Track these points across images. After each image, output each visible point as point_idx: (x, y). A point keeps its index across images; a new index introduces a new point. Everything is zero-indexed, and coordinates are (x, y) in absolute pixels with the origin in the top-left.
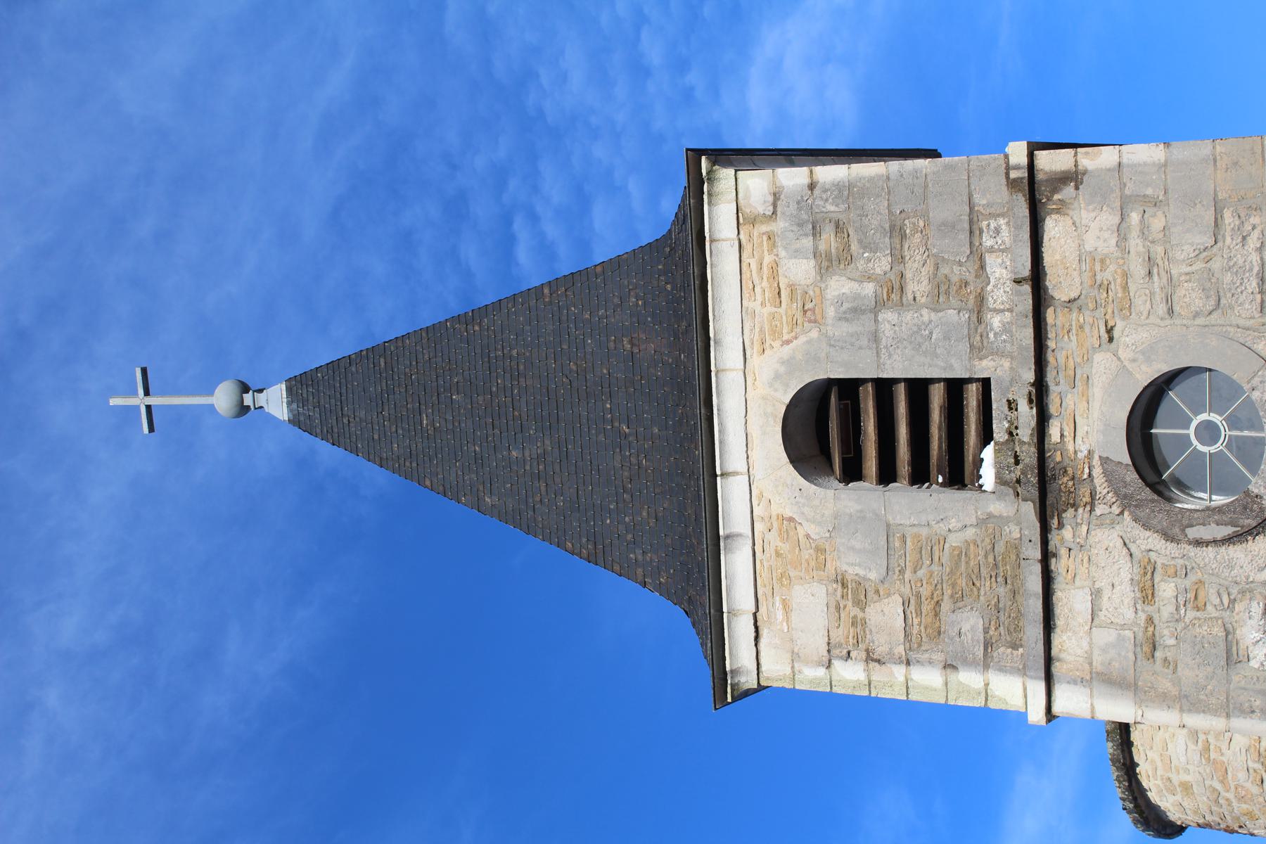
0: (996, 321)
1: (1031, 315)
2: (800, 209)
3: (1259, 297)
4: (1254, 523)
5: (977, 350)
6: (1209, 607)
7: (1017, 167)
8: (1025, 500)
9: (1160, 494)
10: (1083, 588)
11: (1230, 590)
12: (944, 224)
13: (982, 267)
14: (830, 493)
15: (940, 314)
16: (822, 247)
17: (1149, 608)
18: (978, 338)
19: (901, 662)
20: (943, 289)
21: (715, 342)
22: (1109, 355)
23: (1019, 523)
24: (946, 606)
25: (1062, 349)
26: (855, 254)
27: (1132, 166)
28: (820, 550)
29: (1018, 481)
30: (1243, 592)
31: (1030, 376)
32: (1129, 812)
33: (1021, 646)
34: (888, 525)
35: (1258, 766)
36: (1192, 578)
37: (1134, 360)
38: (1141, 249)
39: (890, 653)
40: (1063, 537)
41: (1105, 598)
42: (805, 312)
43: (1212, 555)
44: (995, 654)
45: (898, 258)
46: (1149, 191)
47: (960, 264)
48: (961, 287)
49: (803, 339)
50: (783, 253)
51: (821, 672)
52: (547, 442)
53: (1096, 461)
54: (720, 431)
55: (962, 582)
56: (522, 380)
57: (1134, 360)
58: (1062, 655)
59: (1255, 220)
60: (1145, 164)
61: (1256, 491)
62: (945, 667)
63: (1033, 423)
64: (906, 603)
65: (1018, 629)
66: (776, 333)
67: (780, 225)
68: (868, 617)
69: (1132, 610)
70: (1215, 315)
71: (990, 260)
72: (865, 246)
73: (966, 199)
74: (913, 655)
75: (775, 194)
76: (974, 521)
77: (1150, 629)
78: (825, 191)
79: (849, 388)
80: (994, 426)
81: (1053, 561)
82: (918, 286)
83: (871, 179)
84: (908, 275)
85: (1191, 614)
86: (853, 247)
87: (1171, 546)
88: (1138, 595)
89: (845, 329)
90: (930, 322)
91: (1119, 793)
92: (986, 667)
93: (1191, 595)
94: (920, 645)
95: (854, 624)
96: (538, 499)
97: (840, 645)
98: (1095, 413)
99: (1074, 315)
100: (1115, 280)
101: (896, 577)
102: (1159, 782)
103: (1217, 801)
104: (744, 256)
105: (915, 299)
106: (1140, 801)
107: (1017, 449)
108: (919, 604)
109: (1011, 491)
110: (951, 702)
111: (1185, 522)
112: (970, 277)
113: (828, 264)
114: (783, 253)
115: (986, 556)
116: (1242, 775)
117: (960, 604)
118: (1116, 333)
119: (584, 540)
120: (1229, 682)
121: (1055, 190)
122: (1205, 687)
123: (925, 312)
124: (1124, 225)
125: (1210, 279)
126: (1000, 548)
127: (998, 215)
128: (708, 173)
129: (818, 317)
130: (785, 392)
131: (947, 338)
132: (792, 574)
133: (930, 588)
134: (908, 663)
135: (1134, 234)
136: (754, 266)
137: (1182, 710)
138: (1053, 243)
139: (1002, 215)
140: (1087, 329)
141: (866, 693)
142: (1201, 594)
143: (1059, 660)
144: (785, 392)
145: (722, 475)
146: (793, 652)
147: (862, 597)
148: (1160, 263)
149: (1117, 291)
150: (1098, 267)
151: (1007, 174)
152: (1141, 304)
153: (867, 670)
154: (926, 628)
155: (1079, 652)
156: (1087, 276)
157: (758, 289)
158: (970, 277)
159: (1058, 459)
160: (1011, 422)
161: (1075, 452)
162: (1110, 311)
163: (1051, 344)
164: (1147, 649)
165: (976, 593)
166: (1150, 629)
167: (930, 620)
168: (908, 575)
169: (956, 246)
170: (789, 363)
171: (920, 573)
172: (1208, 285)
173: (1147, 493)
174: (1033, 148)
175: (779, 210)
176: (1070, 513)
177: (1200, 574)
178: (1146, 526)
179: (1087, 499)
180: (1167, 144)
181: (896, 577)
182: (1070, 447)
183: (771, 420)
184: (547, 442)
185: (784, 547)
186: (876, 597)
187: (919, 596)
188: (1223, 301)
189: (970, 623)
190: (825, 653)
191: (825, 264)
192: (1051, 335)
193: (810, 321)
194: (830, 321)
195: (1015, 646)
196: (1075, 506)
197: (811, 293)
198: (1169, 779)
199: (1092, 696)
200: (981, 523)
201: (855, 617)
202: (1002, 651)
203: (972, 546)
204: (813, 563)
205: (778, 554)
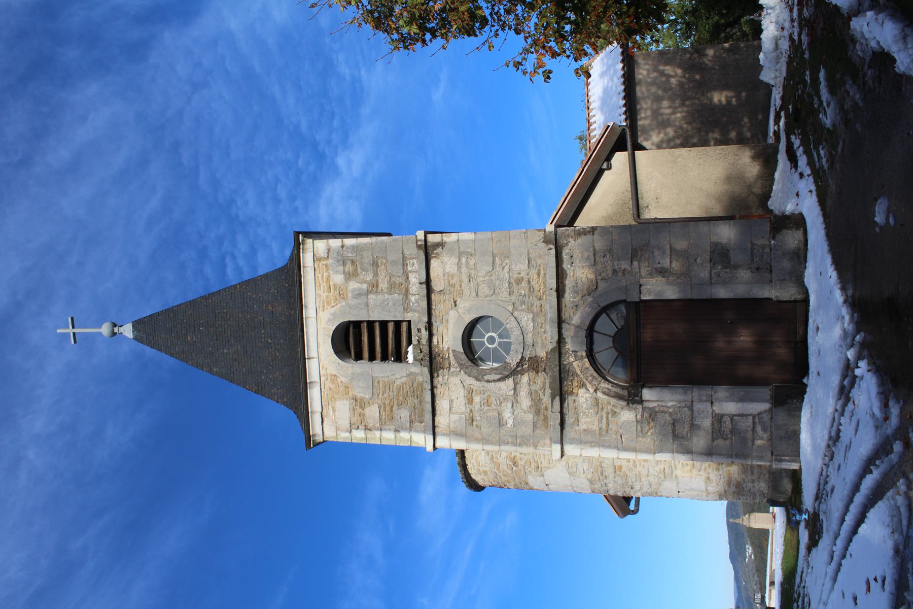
0: (413, 299)
1: (426, 296)
2: (338, 255)
3: (509, 290)
4: (508, 373)
5: (406, 309)
6: (493, 405)
7: (420, 240)
8: (424, 366)
9: (474, 363)
10: (446, 399)
11: (500, 398)
12: (393, 261)
13: (408, 278)
14: (350, 365)
15: (392, 296)
16: (347, 270)
17: (471, 406)
18: (406, 305)
19: (378, 430)
20: (393, 286)
21: (305, 307)
22: (455, 311)
23: (422, 375)
24: (395, 408)
25: (437, 309)
26: (359, 272)
27: (463, 241)
28: (347, 387)
29: (422, 359)
30: (504, 399)
31: (426, 319)
32: (465, 483)
33: (424, 422)
34: (373, 377)
35: (511, 463)
36: (486, 394)
37: (464, 313)
38: (466, 271)
39: (374, 426)
40: (439, 380)
41: (455, 403)
42: (340, 295)
43: (493, 386)
44: (414, 425)
45: (376, 274)
46: (469, 250)
47: (399, 277)
48: (399, 285)
49: (339, 305)
50: (331, 272)
51: (348, 434)
52: (239, 346)
53: (451, 351)
54: (307, 342)
55: (401, 398)
56: (228, 322)
57: (464, 313)
58: (439, 425)
59: (507, 261)
60: (467, 240)
61: (509, 361)
62: (395, 431)
63: (427, 337)
64: (380, 407)
65: (422, 416)
66: (328, 303)
67: (330, 261)
68: (365, 413)
69: (465, 407)
70: (493, 296)
71: (410, 275)
72: (363, 270)
73: (401, 252)
74: (382, 427)
75: (328, 249)
76: (405, 375)
77: (471, 414)
78: (348, 248)
79: (357, 324)
80: (413, 339)
81: (435, 389)
82: (383, 285)
83: (365, 244)
84: (380, 281)
85: (486, 408)
86: (358, 270)
87: (478, 383)
88: (467, 401)
89: (356, 301)
90: (388, 299)
91: (461, 476)
92: (411, 430)
93: (486, 401)
94: (385, 423)
95: (360, 415)
96: (235, 368)
97: (355, 424)
98: (450, 334)
99: (442, 296)
100: (457, 283)
101: (376, 397)
102: (475, 471)
103: (496, 477)
104: (317, 272)
105: (382, 290)
106: (468, 478)
107: (421, 347)
108: (385, 407)
109: (419, 363)
110: (398, 444)
111: (483, 373)
112: (403, 282)
113: (349, 276)
114: (331, 272)
115: (410, 388)
116: (505, 467)
117: (401, 407)
118: (457, 303)
119: (254, 385)
120: (500, 432)
121: (435, 249)
122: (491, 435)
123: (386, 295)
124: (460, 263)
125: (491, 283)
126: (415, 385)
127: (413, 258)
128: (302, 241)
129: (345, 297)
130: (333, 326)
131: (394, 305)
132: (336, 396)
133: (389, 401)
134: (381, 430)
135: (464, 266)
136: (320, 277)
137: (483, 444)
138: (434, 269)
139: (415, 258)
140: (447, 301)
141: (365, 442)
142: (489, 400)
143: (438, 427)
144: (333, 326)
145: (308, 358)
146: (336, 427)
147: (363, 405)
148: (473, 277)
149: (457, 286)
150: (450, 278)
151: (417, 243)
152: (466, 292)
153: (365, 433)
154: (387, 416)
155: (445, 423)
156: (446, 281)
157: (322, 286)
158: (403, 282)
159: (437, 351)
160: (419, 337)
161: (443, 348)
162: (455, 295)
163: (434, 307)
164: (470, 421)
165: (406, 402)
166: (471, 414)
167: (389, 413)
168: (381, 396)
169: (398, 270)
170: (334, 315)
171: (385, 395)
172: (490, 285)
173: (469, 363)
174: (426, 233)
175: (330, 255)
176: (441, 371)
177: (489, 393)
178: (469, 376)
179: (447, 366)
180: (475, 233)
181: (376, 397)
182: (441, 346)
183: (327, 337)
184: (239, 346)
185: (333, 386)
186: (368, 405)
187: (384, 404)
188: (496, 291)
189: (404, 414)
190: (349, 427)
191: (348, 276)
192: (433, 304)
193: (342, 299)
194: (349, 298)
195: (421, 422)
196: (443, 368)
197: (342, 287)
198: (479, 470)
199: (450, 440)
200: (408, 375)
201: (360, 413)
202: (416, 424)
203: (405, 385)
204: (344, 392)
205: (330, 389)
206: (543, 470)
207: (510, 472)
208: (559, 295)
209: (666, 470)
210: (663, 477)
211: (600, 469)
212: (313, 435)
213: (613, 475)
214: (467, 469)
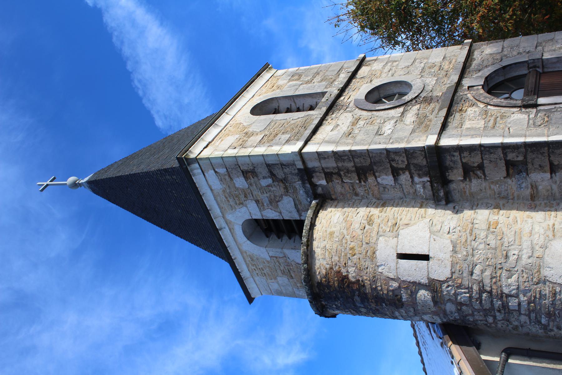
35: (366, 222)
206: (401, 227)
207: (360, 232)
208: (465, 66)
209: (556, 227)
210: (551, 236)
211: (470, 225)
212: (190, 151)
213: (485, 233)
214: (313, 229)
